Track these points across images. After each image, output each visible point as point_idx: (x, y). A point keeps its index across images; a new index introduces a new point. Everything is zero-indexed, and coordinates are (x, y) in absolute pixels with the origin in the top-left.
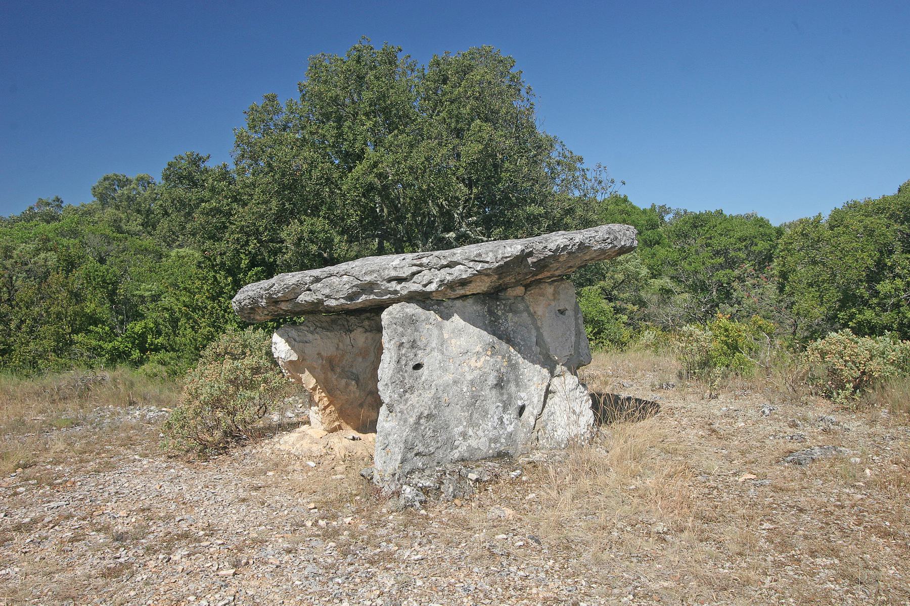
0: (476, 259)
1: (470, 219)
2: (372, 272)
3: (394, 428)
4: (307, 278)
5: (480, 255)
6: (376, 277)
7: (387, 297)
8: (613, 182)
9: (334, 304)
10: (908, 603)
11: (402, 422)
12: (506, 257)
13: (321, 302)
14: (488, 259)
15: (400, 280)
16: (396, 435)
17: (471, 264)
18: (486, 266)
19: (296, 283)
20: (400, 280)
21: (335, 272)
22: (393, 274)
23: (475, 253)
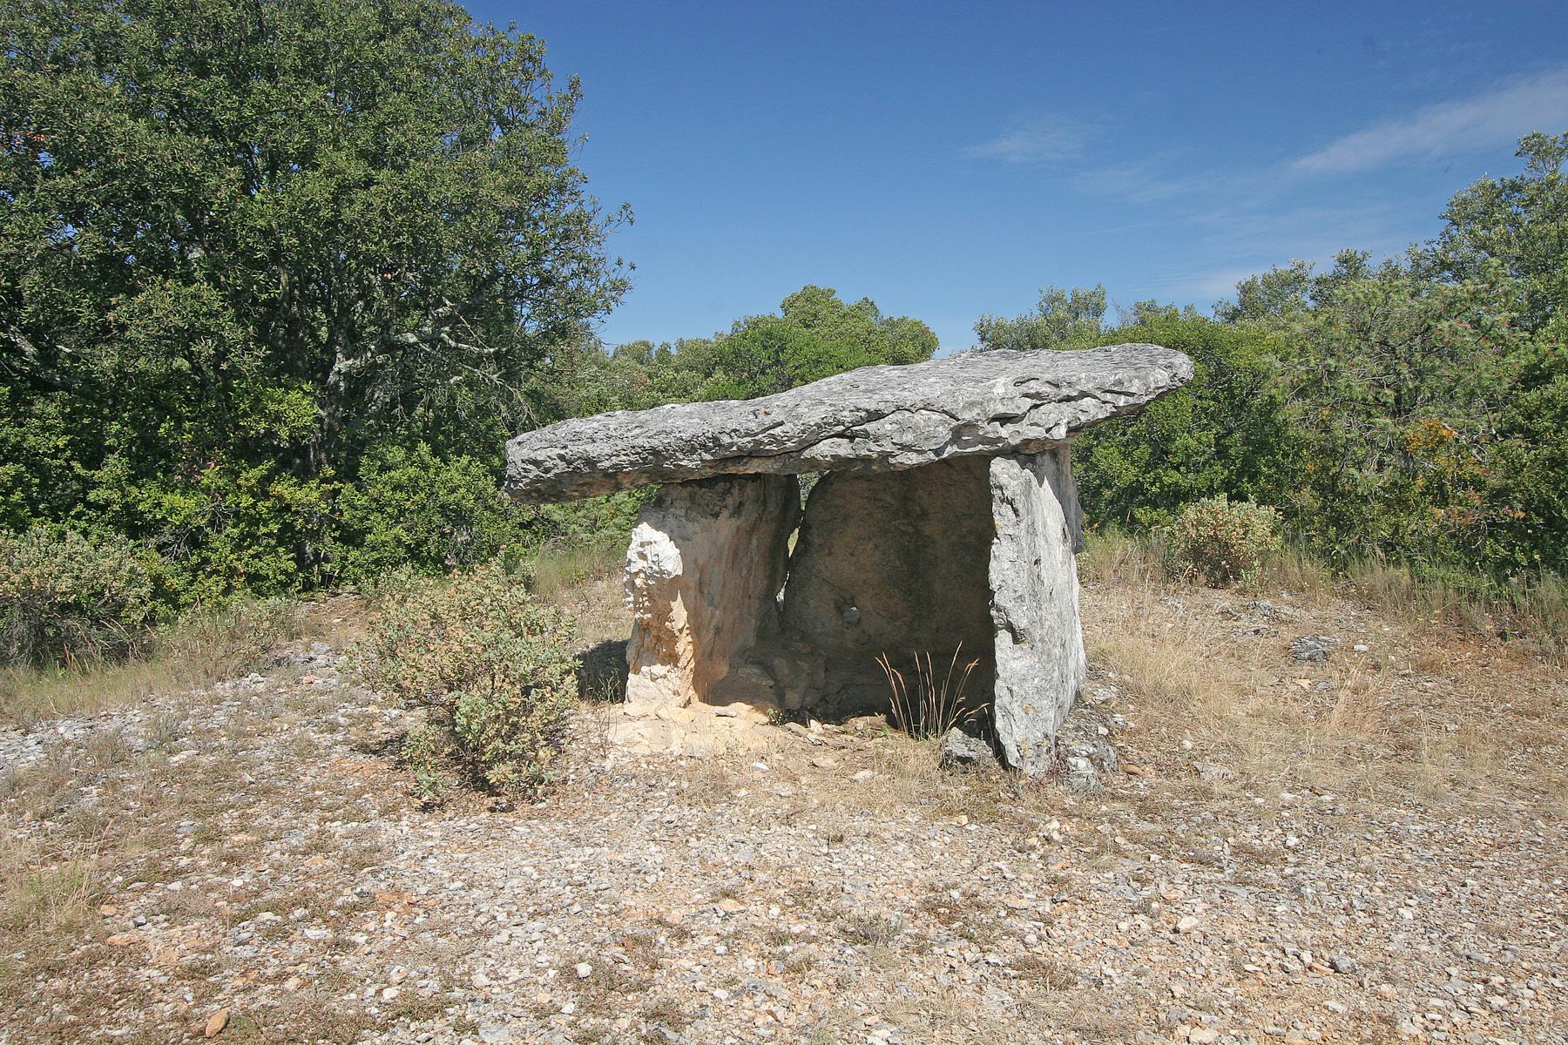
0: (1116, 389)
1: (440, 310)
2: (972, 404)
3: (1032, 667)
4: (846, 413)
5: (1120, 382)
6: (979, 414)
7: (977, 449)
8: (619, 263)
9: (914, 462)
10: (1564, 692)
11: (1045, 657)
12: (1160, 388)
13: (885, 456)
14: (1133, 390)
15: (1004, 419)
16: (1036, 680)
17: (1109, 397)
18: (1131, 400)
19: (820, 421)
20: (1004, 419)
21: (909, 403)
22: (1001, 409)
23: (1112, 378)
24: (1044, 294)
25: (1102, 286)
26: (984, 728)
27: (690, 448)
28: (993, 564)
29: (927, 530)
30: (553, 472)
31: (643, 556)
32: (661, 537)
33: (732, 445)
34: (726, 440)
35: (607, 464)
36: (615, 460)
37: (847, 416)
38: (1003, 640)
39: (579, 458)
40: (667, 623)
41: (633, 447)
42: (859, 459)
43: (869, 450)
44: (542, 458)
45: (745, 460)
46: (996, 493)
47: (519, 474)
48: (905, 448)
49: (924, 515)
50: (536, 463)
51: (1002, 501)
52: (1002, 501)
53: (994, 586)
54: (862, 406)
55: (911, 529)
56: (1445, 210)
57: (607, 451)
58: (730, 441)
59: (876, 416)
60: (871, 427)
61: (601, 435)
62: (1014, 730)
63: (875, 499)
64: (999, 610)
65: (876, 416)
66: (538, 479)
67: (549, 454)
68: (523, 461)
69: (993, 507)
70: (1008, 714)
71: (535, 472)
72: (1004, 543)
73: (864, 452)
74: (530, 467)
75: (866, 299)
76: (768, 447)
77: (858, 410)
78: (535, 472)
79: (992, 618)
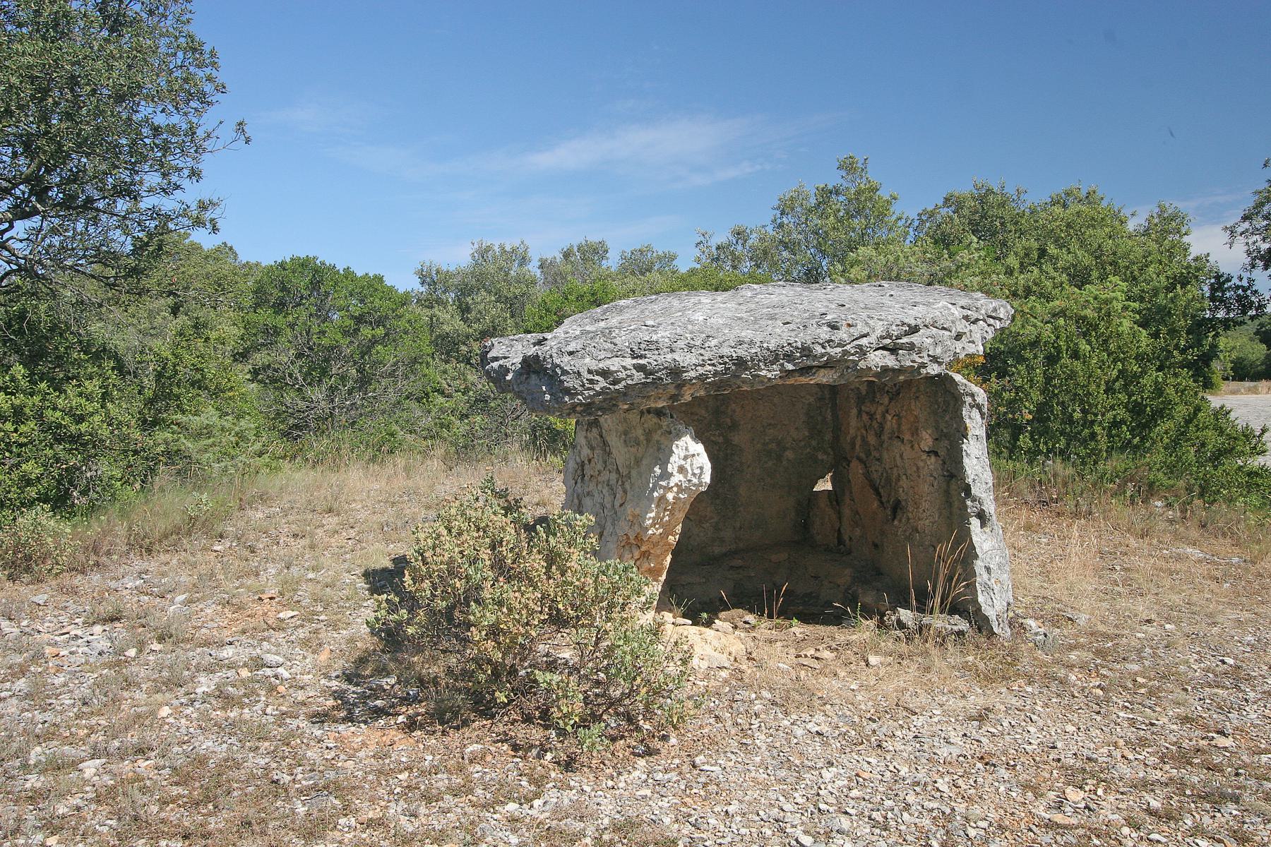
0: (994, 314)
16: (997, 557)
24: (476, 246)
25: (525, 243)
26: (965, 607)
27: (774, 357)
28: (966, 461)
29: (736, 439)
30: (623, 383)
31: (682, 469)
32: (699, 448)
33: (823, 355)
34: (819, 350)
35: (693, 374)
36: (701, 370)
37: (895, 331)
38: (975, 523)
39: (666, 368)
40: (670, 537)
41: (722, 357)
42: (901, 370)
43: (913, 361)
44: (615, 369)
45: (814, 370)
46: (968, 400)
47: (583, 386)
48: (935, 359)
49: (734, 426)
50: (605, 373)
51: (972, 407)
52: (972, 407)
53: (969, 481)
54: (906, 321)
55: (721, 440)
56: (776, 203)
57: (694, 361)
58: (823, 351)
59: (914, 330)
60: (915, 338)
61: (681, 344)
62: (993, 604)
63: (692, 414)
64: (974, 500)
65: (914, 330)
66: (603, 391)
67: (624, 364)
68: (590, 372)
69: (964, 412)
70: (988, 588)
71: (602, 383)
72: (971, 442)
73: (909, 363)
74: (597, 378)
75: (225, 244)
76: (851, 358)
77: (903, 324)
78: (602, 383)
79: (966, 507)
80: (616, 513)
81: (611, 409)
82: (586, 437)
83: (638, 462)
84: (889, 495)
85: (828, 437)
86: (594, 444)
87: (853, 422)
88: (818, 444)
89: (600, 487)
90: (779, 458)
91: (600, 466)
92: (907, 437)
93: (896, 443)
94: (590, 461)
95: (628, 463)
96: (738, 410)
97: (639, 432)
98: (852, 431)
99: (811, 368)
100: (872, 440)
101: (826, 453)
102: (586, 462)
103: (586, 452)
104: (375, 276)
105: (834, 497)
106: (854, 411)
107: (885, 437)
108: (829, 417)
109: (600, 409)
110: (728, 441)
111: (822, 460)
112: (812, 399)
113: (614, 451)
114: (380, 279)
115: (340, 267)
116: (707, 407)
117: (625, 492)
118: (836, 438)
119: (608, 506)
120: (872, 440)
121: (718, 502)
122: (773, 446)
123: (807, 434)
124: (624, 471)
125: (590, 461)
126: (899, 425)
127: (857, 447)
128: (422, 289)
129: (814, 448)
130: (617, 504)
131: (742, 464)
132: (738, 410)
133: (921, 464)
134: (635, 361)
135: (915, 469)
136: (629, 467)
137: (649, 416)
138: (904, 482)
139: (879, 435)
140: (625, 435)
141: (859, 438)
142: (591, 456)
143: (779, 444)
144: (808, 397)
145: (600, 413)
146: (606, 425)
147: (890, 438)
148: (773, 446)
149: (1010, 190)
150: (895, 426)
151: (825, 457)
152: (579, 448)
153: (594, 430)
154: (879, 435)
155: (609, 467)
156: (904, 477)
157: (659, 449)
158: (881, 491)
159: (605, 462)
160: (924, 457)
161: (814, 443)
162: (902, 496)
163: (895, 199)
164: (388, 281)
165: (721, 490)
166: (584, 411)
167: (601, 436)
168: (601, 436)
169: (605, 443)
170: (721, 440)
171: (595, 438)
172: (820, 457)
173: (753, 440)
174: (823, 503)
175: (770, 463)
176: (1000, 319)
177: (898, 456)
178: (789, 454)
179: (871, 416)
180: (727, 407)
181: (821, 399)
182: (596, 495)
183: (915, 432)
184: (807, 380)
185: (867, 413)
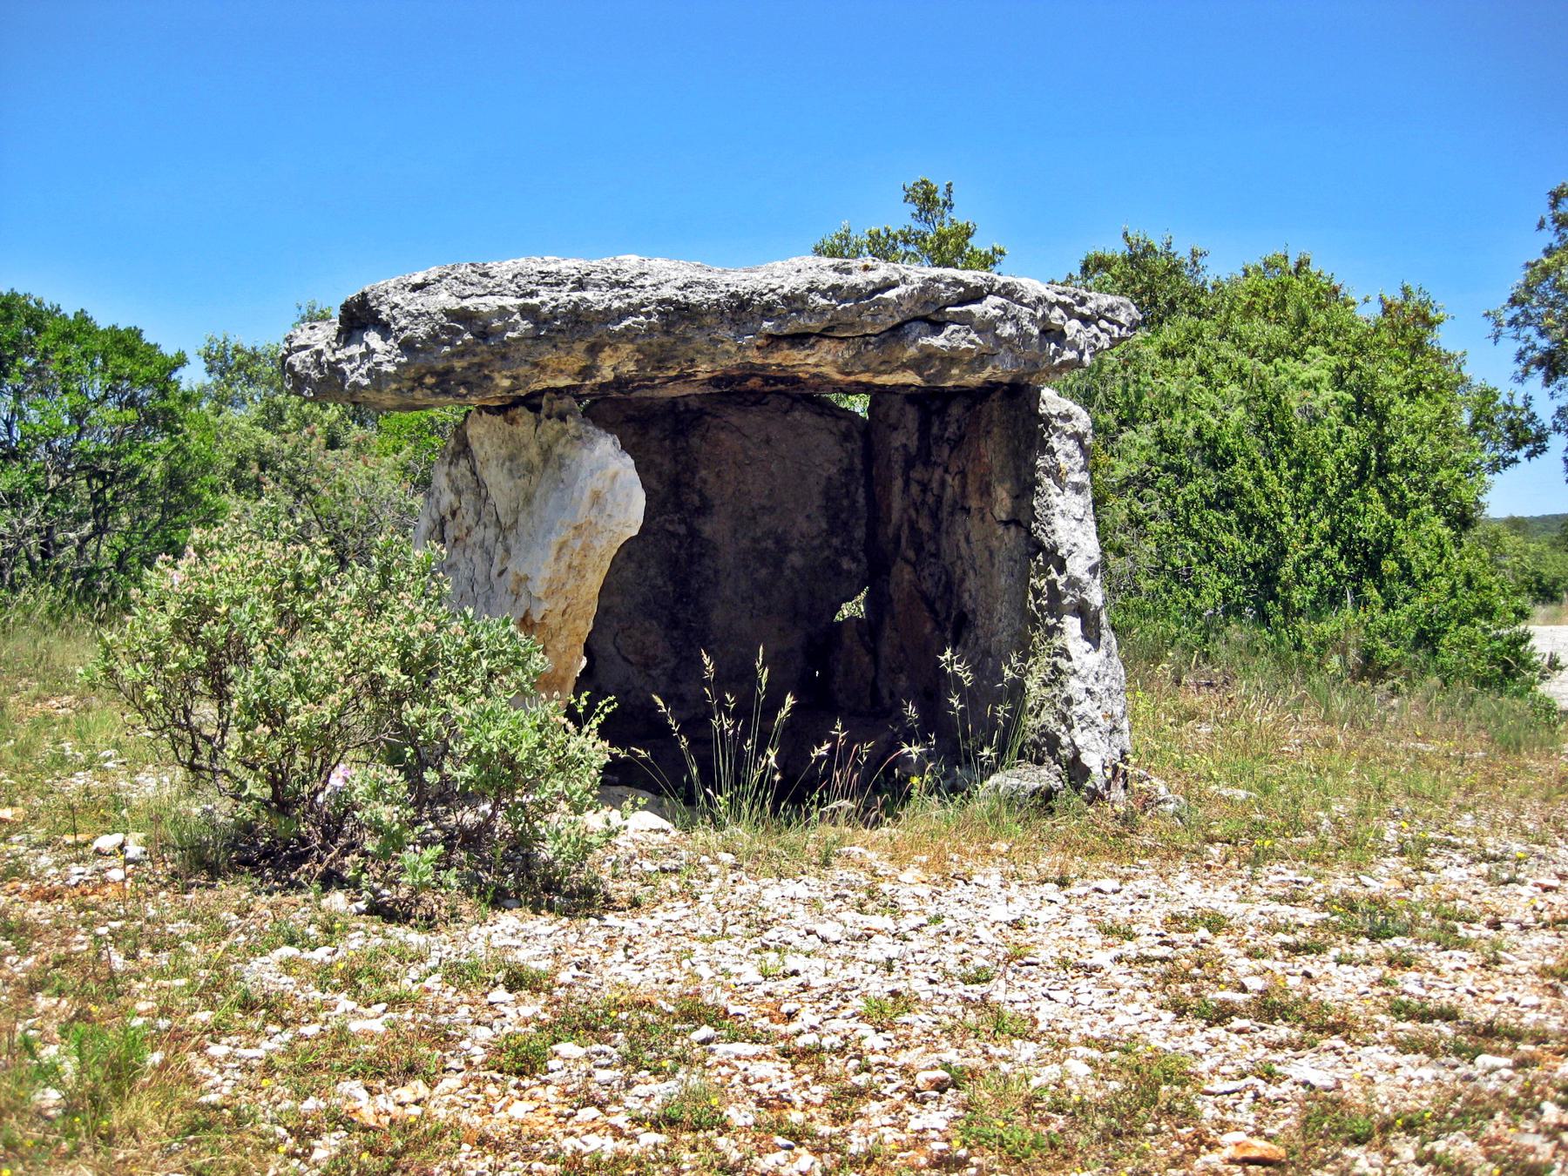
29: (708, 528)
32: (624, 468)
45: (812, 340)
49: (704, 509)
55: (682, 530)
80: (492, 588)
81: (480, 386)
82: (448, 475)
83: (529, 500)
84: (949, 607)
85: (860, 533)
86: (461, 485)
87: (897, 503)
88: (843, 543)
89: (468, 553)
90: (778, 565)
91: (470, 520)
92: (974, 503)
93: (959, 517)
94: (454, 514)
95: (514, 505)
96: (711, 479)
97: (533, 453)
98: (895, 516)
99: (807, 336)
100: (925, 525)
101: (855, 559)
102: (449, 517)
103: (448, 498)
104: (129, 330)
105: (869, 628)
106: (898, 484)
107: (944, 514)
108: (861, 500)
109: (464, 383)
110: (693, 533)
111: (849, 572)
112: (833, 470)
113: (493, 492)
114: (136, 334)
115: (69, 311)
116: (660, 474)
117: (507, 550)
118: (872, 535)
119: (481, 578)
120: (925, 525)
121: (675, 634)
122: (770, 544)
123: (824, 526)
124: (506, 520)
125: (454, 514)
126: (964, 486)
127: (903, 541)
128: (209, 381)
129: (836, 550)
130: (494, 572)
131: (716, 572)
132: (711, 479)
133: (995, 543)
134: (521, 301)
135: (987, 554)
136: (516, 512)
137: (549, 423)
138: (971, 583)
139: (934, 515)
140: (511, 460)
141: (906, 526)
142: (456, 505)
143: (777, 542)
144: (826, 465)
145: (463, 391)
146: (482, 454)
147: (952, 514)
148: (770, 544)
149: (1183, 254)
150: (958, 490)
151: (854, 566)
152: (437, 494)
153: (463, 463)
154: (934, 515)
155: (486, 519)
156: (971, 573)
157: (561, 466)
158: (938, 606)
159: (479, 514)
160: (1000, 530)
161: (836, 542)
162: (970, 605)
163: (1002, 253)
164: (149, 337)
165: (681, 615)
166: (436, 385)
167: (474, 473)
168: (474, 473)
169: (479, 483)
170: (682, 530)
171: (463, 475)
172: (845, 567)
173: (736, 531)
174: (848, 639)
175: (764, 572)
176: (1121, 326)
177: (962, 538)
178: (795, 559)
179: (925, 488)
180: (693, 474)
181: (848, 471)
182: (462, 567)
183: (986, 491)
184: (802, 356)
185: (918, 482)
